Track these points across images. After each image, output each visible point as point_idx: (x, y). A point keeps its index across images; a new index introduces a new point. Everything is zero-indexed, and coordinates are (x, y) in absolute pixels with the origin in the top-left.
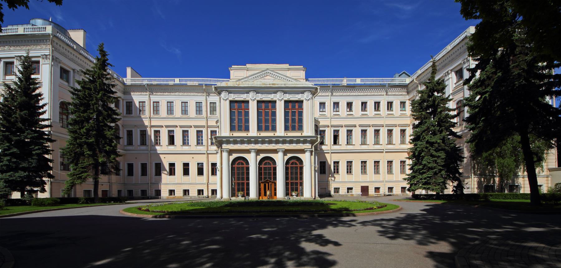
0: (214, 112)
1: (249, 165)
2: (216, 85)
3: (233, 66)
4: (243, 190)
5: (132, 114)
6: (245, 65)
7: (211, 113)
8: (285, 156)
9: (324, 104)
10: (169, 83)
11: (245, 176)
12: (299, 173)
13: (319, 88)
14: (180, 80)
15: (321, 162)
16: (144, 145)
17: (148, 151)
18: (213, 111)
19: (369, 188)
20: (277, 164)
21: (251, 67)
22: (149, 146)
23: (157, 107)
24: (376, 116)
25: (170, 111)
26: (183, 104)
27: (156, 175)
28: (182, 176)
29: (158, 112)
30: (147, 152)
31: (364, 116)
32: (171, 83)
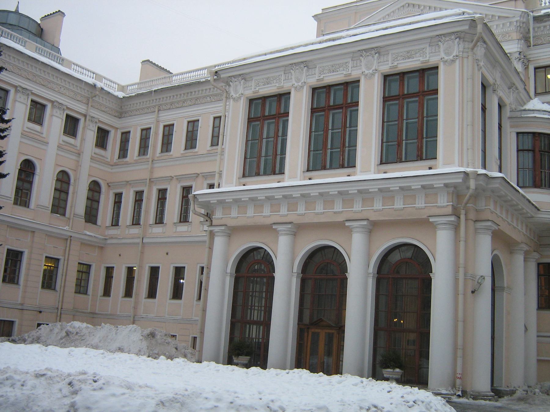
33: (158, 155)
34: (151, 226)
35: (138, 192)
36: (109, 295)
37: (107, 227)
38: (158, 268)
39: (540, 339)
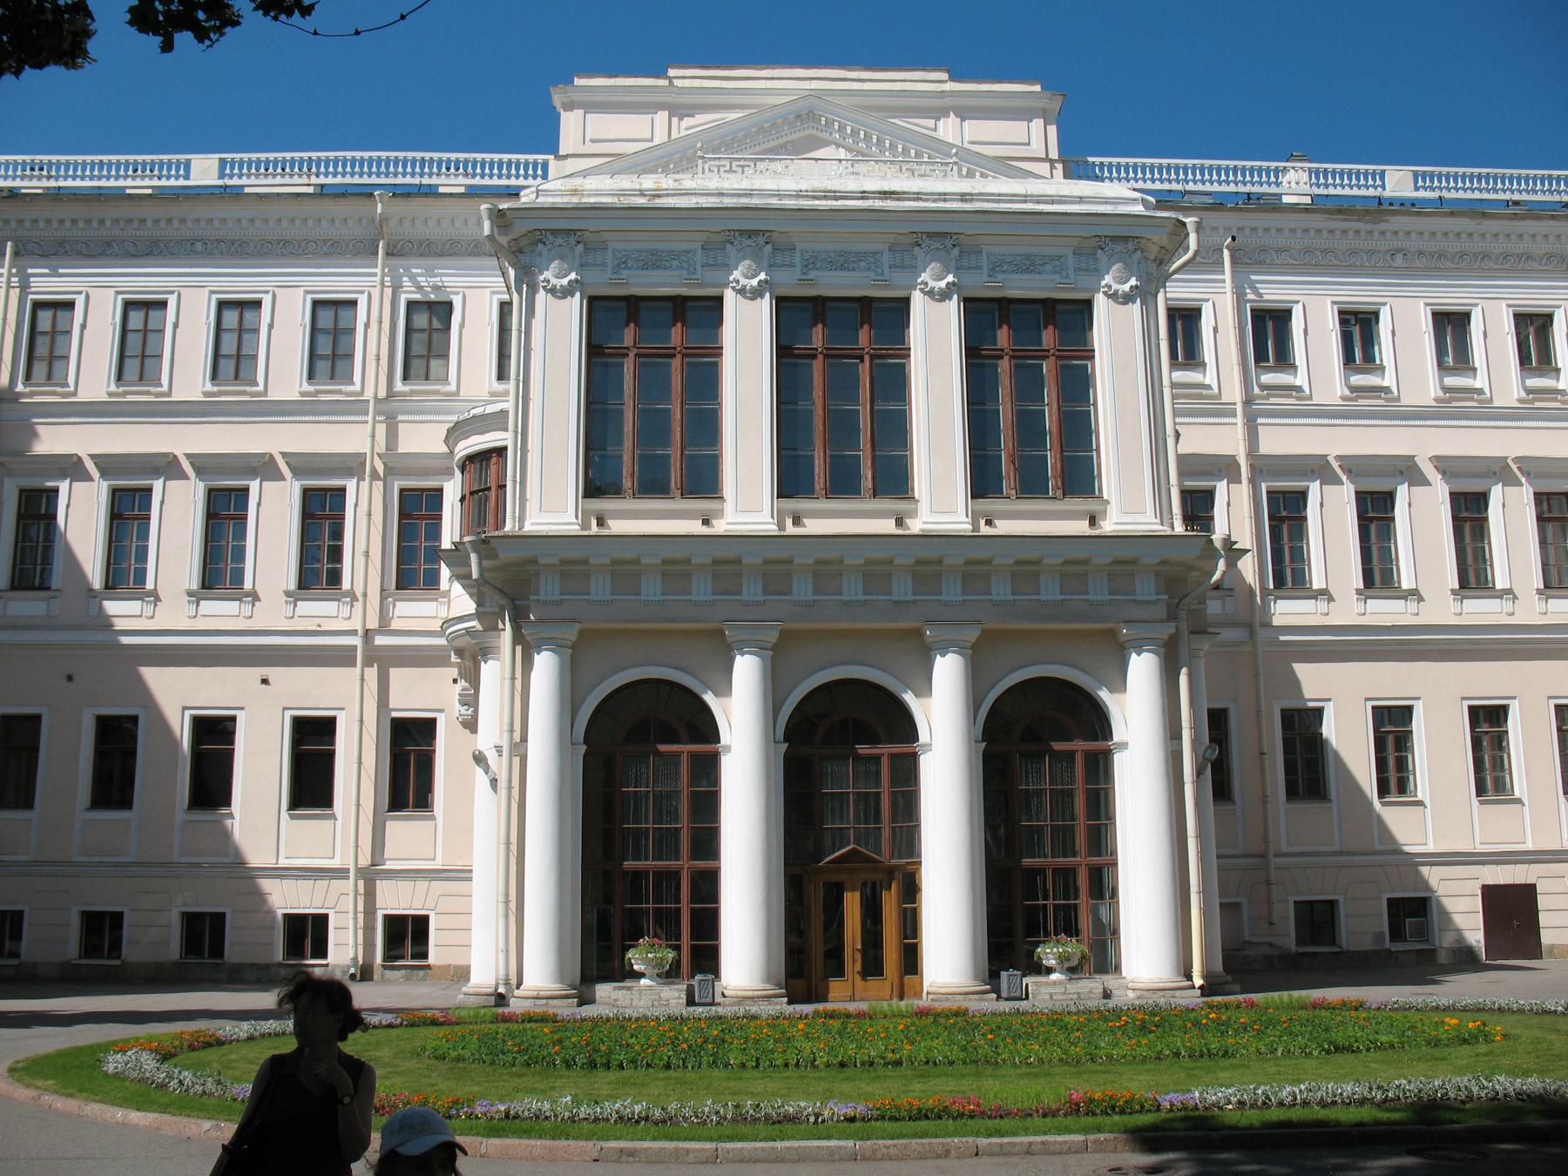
0: (434, 363)
1: (717, 739)
2: (514, 193)
3: (578, 82)
4: (667, 927)
6: (661, 74)
7: (413, 372)
8: (366, 669)
10: (443, 180)
11: (684, 824)
12: (1080, 803)
13: (1190, 221)
14: (223, 162)
16: (33, 588)
18: (428, 358)
19: (1542, 902)
20: (923, 737)
21: (697, 83)
23: (145, 331)
25: (137, 362)
26: (421, 320)
28: (285, 814)
29: (57, 365)
32: (138, 182)
36: (125, 802)
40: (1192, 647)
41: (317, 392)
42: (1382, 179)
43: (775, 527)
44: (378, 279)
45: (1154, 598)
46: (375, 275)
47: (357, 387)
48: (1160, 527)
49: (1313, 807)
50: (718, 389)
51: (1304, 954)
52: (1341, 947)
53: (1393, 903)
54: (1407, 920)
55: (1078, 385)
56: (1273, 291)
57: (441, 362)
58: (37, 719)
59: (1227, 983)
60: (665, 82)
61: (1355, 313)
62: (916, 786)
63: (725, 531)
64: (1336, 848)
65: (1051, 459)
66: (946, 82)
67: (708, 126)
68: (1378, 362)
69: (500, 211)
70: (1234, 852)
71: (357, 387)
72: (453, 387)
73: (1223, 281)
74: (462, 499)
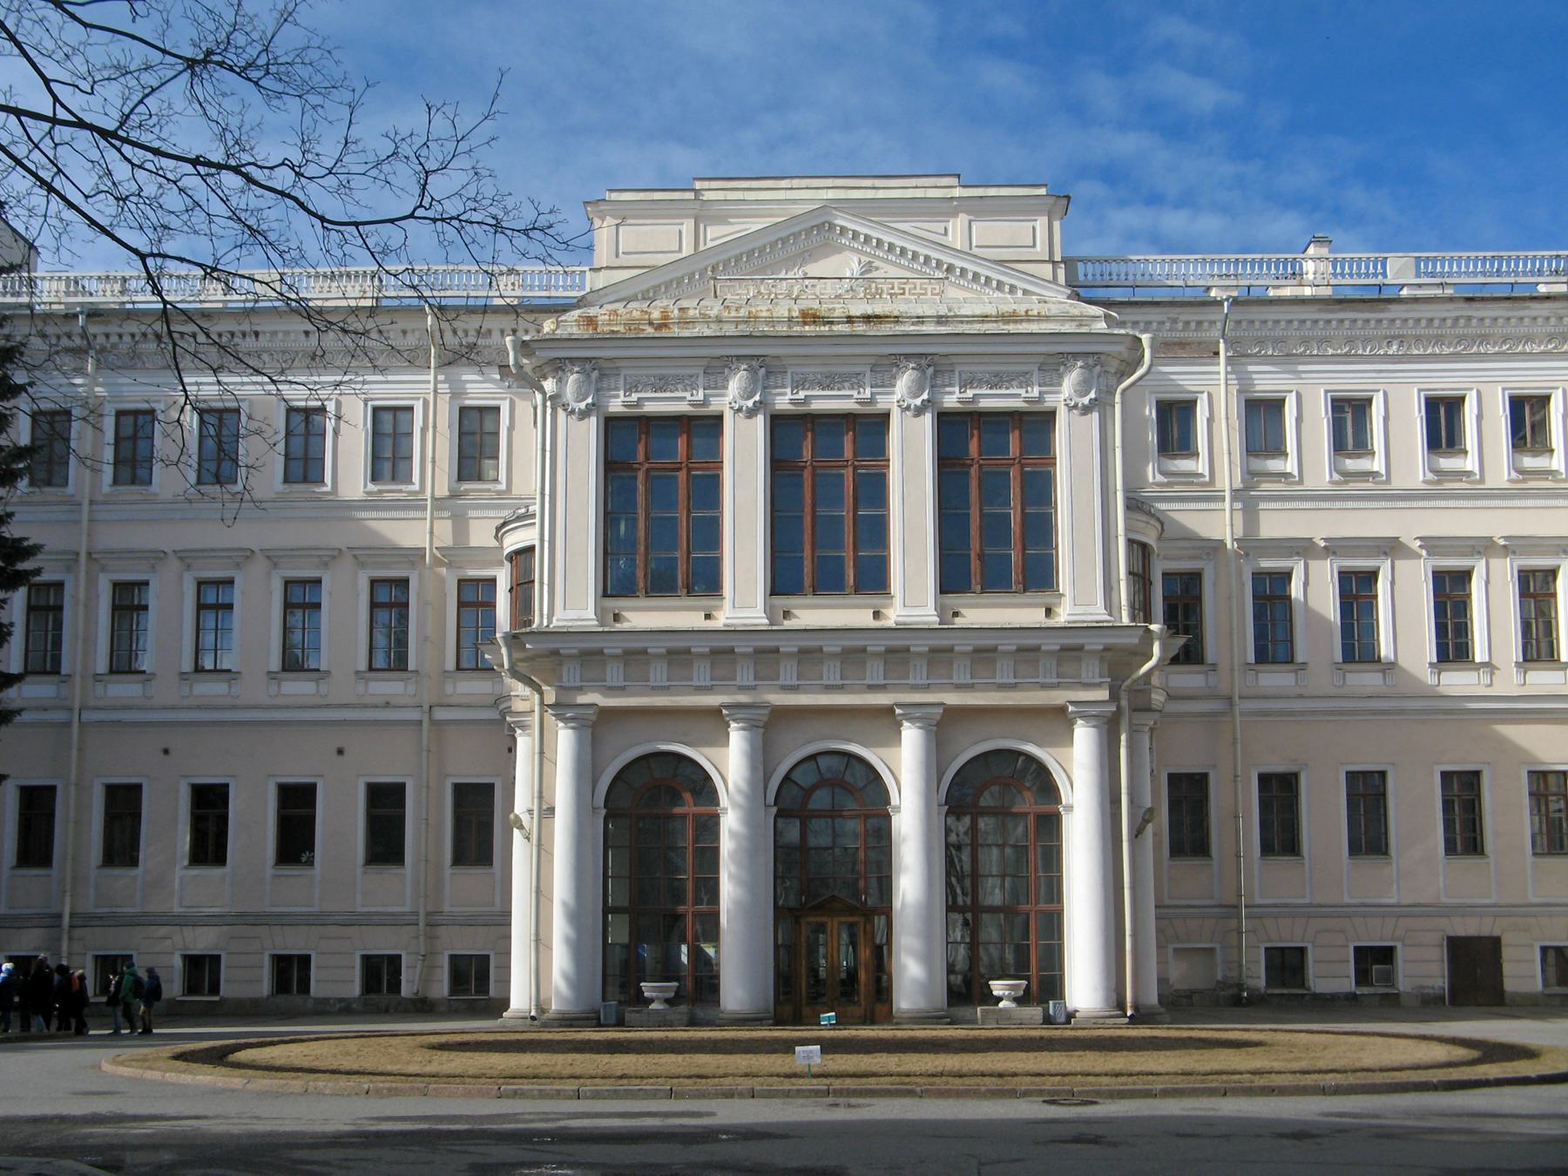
5: (66, 484)
9: (1453, 405)
13: (1145, 338)
15: (1174, 779)
17: (70, 709)
19: (1506, 953)
22: (78, 679)
24: (1531, 484)
27: (461, 857)
28: (448, 869)
29: (402, 465)
30: (59, 716)
31: (1441, 488)
33: (106, 489)
34: (185, 677)
35: (292, 582)
36: (220, 859)
37: (269, 672)
38: (138, 787)
39: (1162, 911)
40: (1134, 722)
41: (380, 492)
42: (1384, 267)
43: (766, 621)
44: (431, 386)
45: (1098, 680)
46: (429, 382)
47: (416, 487)
48: (1108, 618)
49: (1470, 862)
50: (718, 494)
51: (1273, 995)
52: (1308, 989)
53: (1360, 952)
54: (1374, 967)
55: (1040, 488)
56: (1267, 381)
57: (491, 462)
58: (138, 787)
59: (1160, 1014)
60: (690, 195)
61: (1349, 401)
62: (1058, 841)
63: (725, 625)
64: (1307, 901)
65: (1015, 556)
66: (955, 187)
67: (739, 235)
68: (1370, 447)
69: (524, 341)
70: (1208, 902)
71: (416, 487)
72: (503, 487)
73: (1219, 373)
74: (511, 590)
